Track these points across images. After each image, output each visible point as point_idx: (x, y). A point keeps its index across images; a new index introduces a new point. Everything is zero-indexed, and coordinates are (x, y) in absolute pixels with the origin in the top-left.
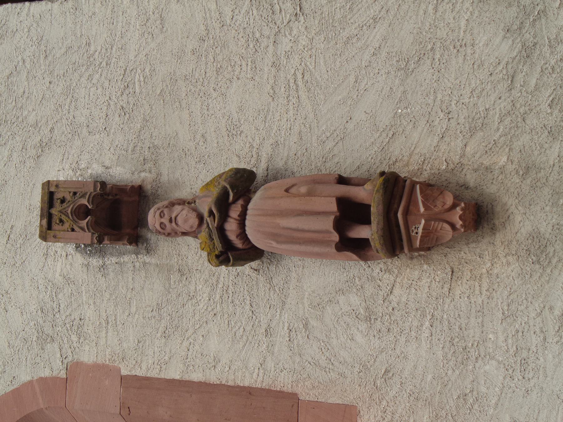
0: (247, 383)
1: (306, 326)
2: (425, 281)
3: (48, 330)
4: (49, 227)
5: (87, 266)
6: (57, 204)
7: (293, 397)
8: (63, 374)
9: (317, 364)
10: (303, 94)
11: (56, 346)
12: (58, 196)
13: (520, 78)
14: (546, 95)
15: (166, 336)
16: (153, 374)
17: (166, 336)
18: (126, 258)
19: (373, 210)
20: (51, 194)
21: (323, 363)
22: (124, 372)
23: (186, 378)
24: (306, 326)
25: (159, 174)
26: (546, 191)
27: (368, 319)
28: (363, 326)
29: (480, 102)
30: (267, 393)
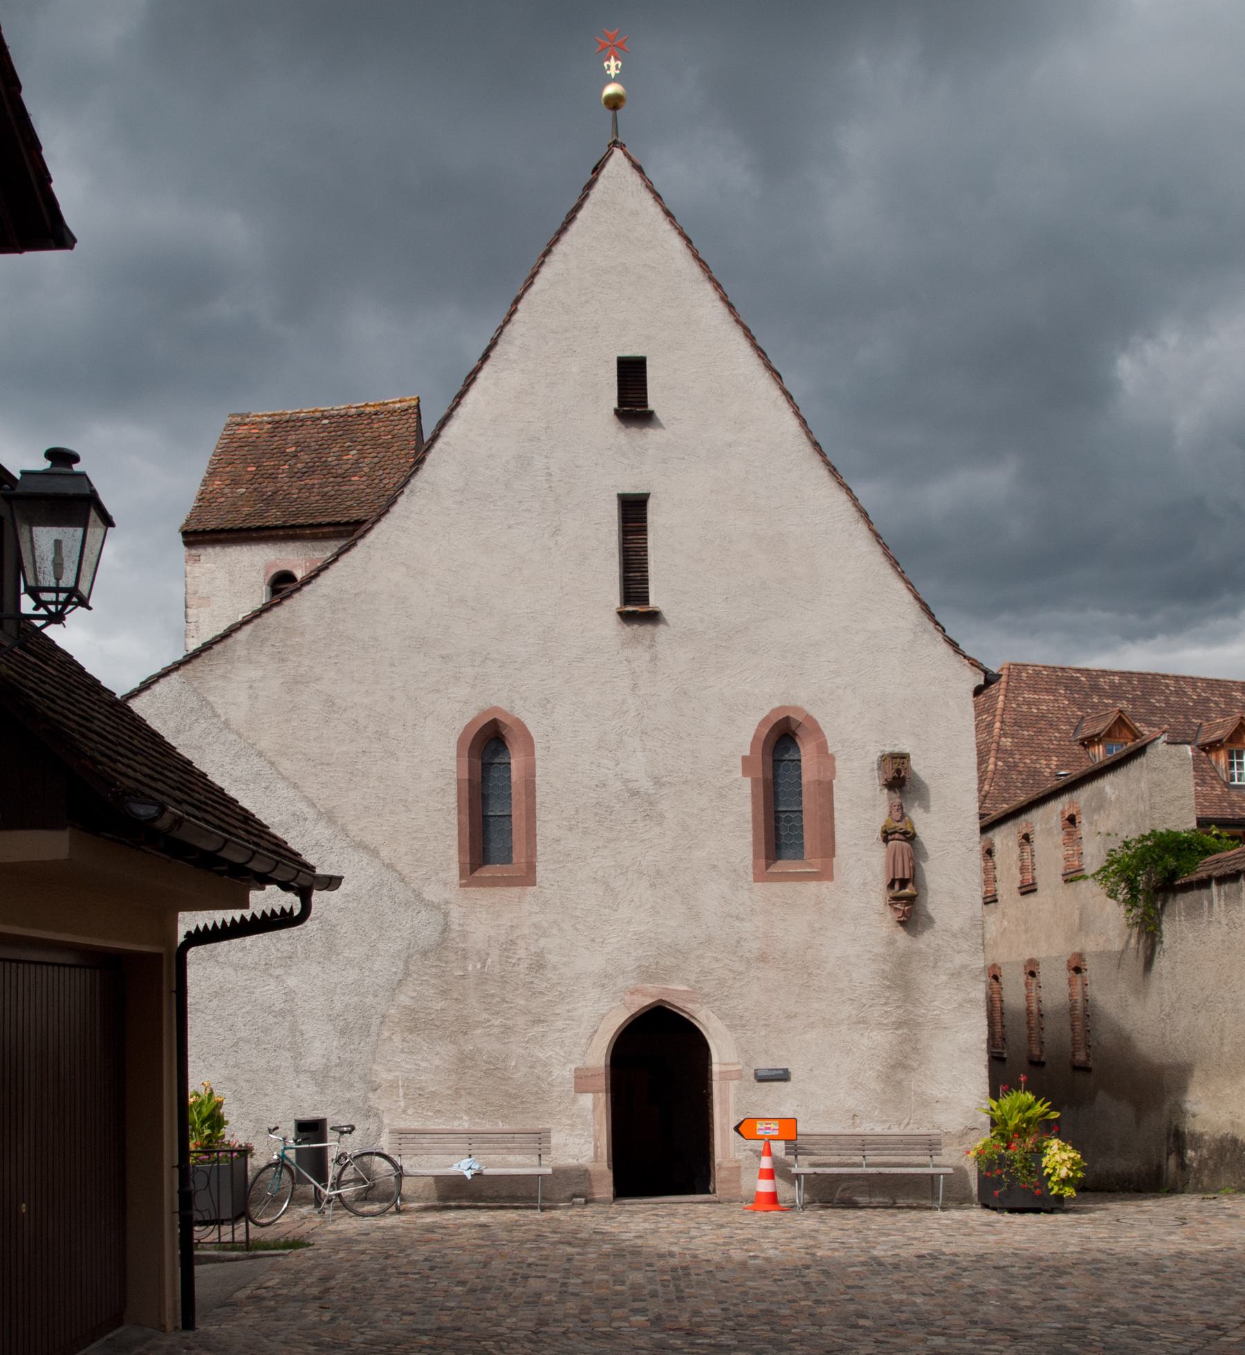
0: (836, 836)
1: (860, 860)
2: (878, 904)
3: (846, 744)
4: (893, 758)
5: (873, 763)
6: (902, 760)
7: (833, 855)
8: (830, 752)
9: (846, 864)
10: (940, 853)
11: (841, 748)
12: (905, 761)
13: (945, 933)
14: (940, 942)
15: (850, 800)
16: (835, 796)
17: (850, 800)
18: (878, 780)
19: (164, 956)
20: (904, 758)
21: (847, 867)
22: (834, 782)
23: (835, 810)
24: (860, 860)
25: (909, 793)
26: (909, 944)
27: (864, 883)
28: (861, 882)
29: (762, 1255)
30: (834, 846)
